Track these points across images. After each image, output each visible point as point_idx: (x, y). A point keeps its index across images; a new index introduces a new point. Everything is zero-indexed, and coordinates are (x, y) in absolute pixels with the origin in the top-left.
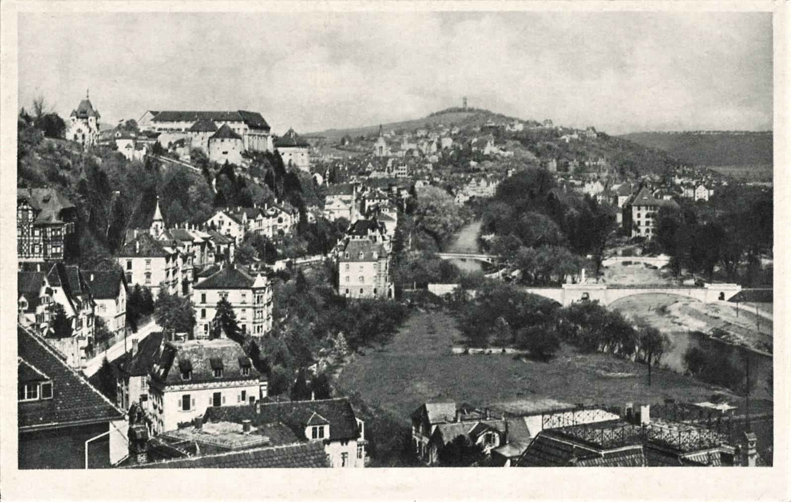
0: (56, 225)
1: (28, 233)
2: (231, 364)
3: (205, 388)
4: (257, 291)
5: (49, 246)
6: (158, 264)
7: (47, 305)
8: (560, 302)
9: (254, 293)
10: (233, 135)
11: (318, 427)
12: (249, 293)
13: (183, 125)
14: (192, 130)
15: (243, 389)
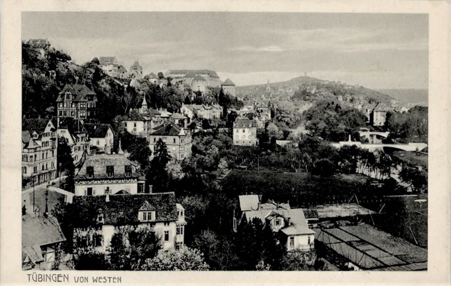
0: (83, 102)
1: (69, 106)
2: (119, 170)
3: (102, 183)
4: (181, 137)
5: (79, 112)
6: (140, 125)
7: (51, 137)
8: (304, 110)
9: (179, 137)
10: (203, 80)
11: (147, 212)
12: (177, 138)
13: (183, 75)
14: (185, 77)
15: (108, 186)
